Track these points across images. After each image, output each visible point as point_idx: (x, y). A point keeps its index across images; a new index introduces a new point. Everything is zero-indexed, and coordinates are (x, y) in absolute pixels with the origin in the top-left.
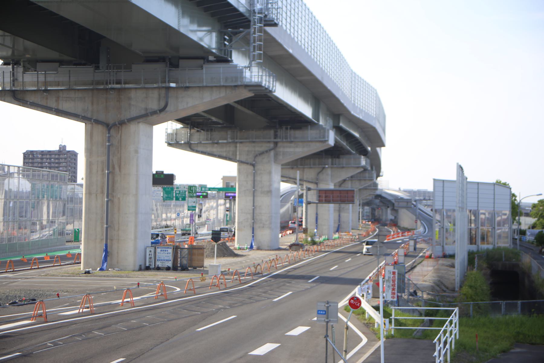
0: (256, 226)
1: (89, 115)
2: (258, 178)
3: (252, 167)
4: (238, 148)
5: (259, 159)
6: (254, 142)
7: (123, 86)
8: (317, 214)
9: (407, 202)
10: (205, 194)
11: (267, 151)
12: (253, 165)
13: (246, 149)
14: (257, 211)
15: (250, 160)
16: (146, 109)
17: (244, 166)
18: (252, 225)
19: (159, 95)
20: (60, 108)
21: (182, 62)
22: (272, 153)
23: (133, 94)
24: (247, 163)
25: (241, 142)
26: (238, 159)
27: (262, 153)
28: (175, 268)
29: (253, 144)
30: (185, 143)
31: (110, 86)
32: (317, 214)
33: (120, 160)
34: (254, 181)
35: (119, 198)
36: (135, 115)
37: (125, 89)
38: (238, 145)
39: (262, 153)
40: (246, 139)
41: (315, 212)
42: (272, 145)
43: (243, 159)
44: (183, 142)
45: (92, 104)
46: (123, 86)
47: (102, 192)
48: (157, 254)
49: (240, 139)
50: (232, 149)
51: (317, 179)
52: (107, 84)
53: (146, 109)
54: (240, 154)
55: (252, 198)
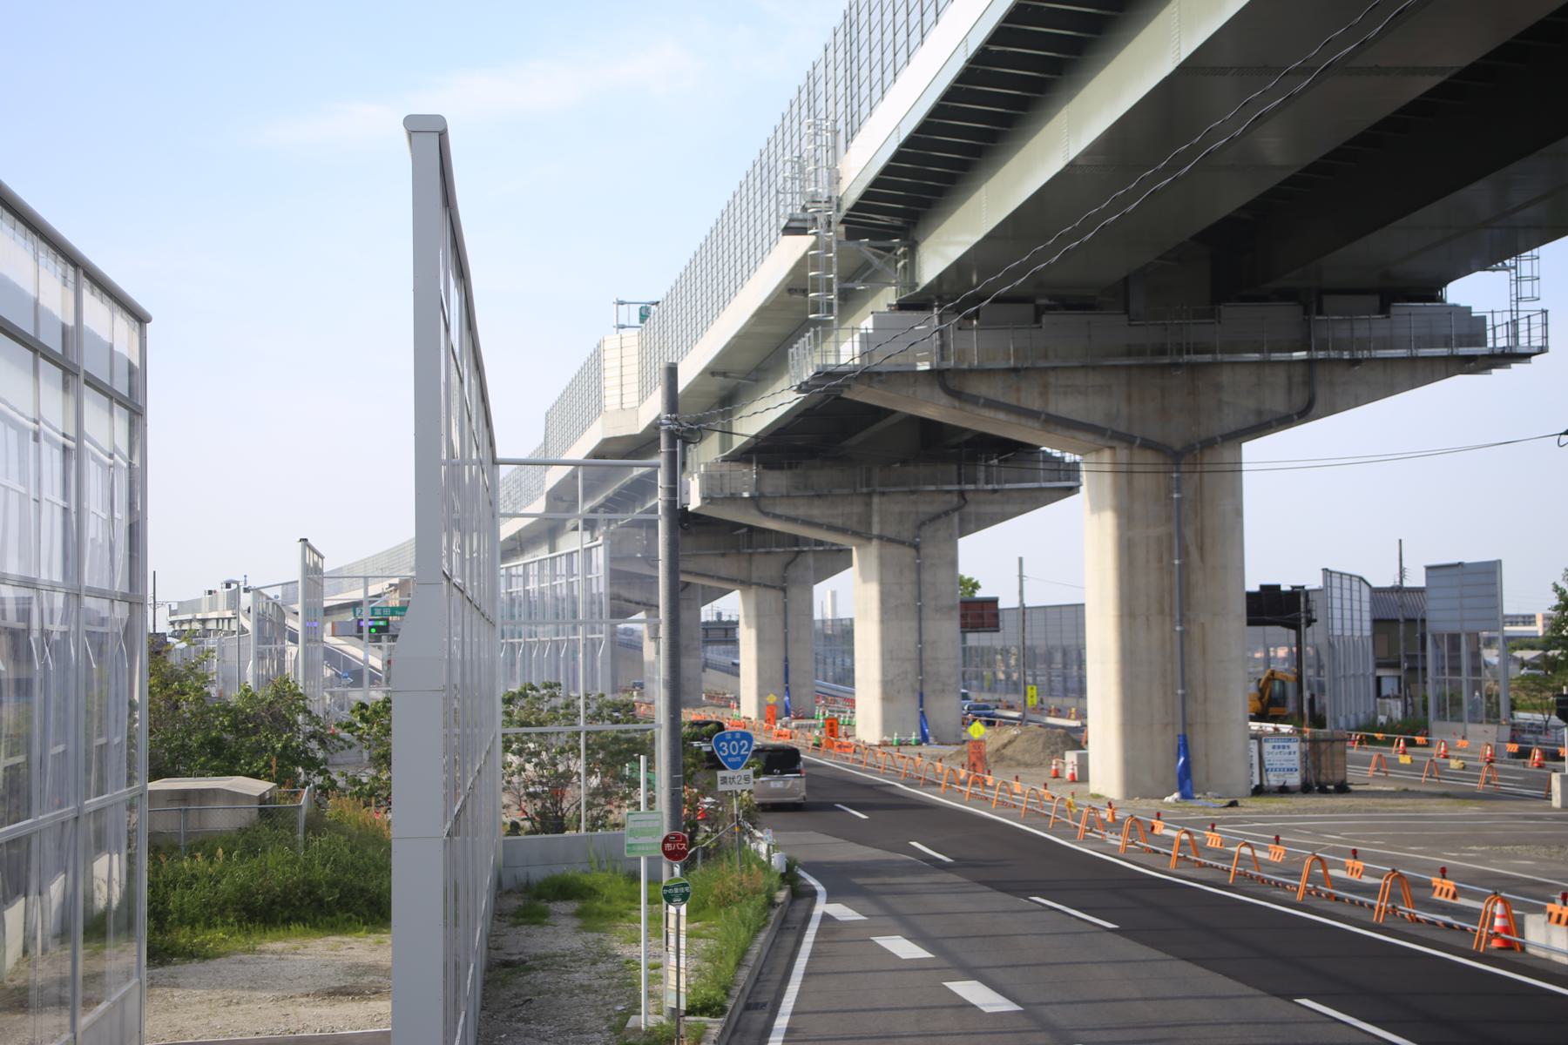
0: (927, 690)
1: (1122, 428)
2: (927, 577)
3: (912, 552)
4: (875, 506)
5: (927, 531)
6: (913, 492)
7: (1219, 357)
8: (786, 660)
9: (726, 630)
10: (382, 623)
11: (946, 513)
12: (917, 547)
13: (896, 509)
14: (928, 654)
15: (906, 535)
16: (1259, 413)
17: (894, 550)
18: (917, 686)
19: (1289, 378)
20: (1052, 409)
21: (1328, 301)
22: (956, 518)
23: (1226, 377)
24: (902, 543)
25: (883, 494)
26: (876, 530)
27: (935, 518)
28: (1306, 789)
29: (914, 497)
30: (751, 498)
31: (1186, 358)
32: (786, 660)
33: (1201, 533)
34: (919, 583)
35: (1203, 625)
36: (1233, 428)
37: (1222, 363)
38: (876, 500)
39: (935, 518)
40: (895, 485)
41: (782, 656)
42: (955, 499)
43: (891, 532)
44: (746, 495)
45: (1129, 399)
46: (1219, 357)
47: (1161, 612)
48: (1266, 756)
49: (882, 485)
50: (856, 508)
51: (784, 579)
52: (1180, 352)
53: (1259, 413)
54: (882, 522)
55: (914, 624)
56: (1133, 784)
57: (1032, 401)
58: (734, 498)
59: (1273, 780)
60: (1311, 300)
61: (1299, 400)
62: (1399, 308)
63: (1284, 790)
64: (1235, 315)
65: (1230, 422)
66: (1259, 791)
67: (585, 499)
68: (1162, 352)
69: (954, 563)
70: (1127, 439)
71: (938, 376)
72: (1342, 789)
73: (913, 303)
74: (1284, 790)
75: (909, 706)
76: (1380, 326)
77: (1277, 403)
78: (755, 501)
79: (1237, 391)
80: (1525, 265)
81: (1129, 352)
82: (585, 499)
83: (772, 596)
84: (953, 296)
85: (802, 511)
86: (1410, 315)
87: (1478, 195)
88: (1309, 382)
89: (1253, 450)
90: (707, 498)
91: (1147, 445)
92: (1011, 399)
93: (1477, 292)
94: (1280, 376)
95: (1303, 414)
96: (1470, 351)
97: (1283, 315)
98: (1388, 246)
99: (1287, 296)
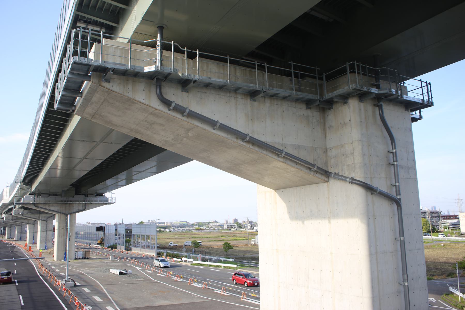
2: (48, 225)
5: (48, 219)
17: (43, 221)
27: (50, 217)
28: (83, 258)
39: (50, 217)
50: (38, 215)
56: (58, 259)
57: (47, 208)
58: (19, 214)
59: (78, 257)
60: (86, 195)
61: (84, 208)
62: (97, 197)
63: (80, 259)
64: (77, 197)
65: (74, 211)
66: (76, 259)
67: (291, 69)
68: (66, 201)
69: (52, 223)
70: (60, 213)
71: (34, 204)
72: (88, 258)
73: (31, 194)
74: (80, 259)
75: (44, 244)
76: (95, 199)
77: (81, 208)
78: (22, 214)
79: (76, 206)
80: (113, 192)
81: (61, 201)
82: (291, 69)
83: (32, 226)
84: (37, 193)
85: (30, 216)
86: (99, 198)
87: (109, 182)
88: (85, 206)
89: (77, 214)
90: (15, 214)
91: (63, 213)
92: (44, 207)
93: (108, 195)
94: (81, 205)
95: (84, 210)
96: (106, 202)
97: (82, 197)
98: (98, 187)
99: (83, 195)
